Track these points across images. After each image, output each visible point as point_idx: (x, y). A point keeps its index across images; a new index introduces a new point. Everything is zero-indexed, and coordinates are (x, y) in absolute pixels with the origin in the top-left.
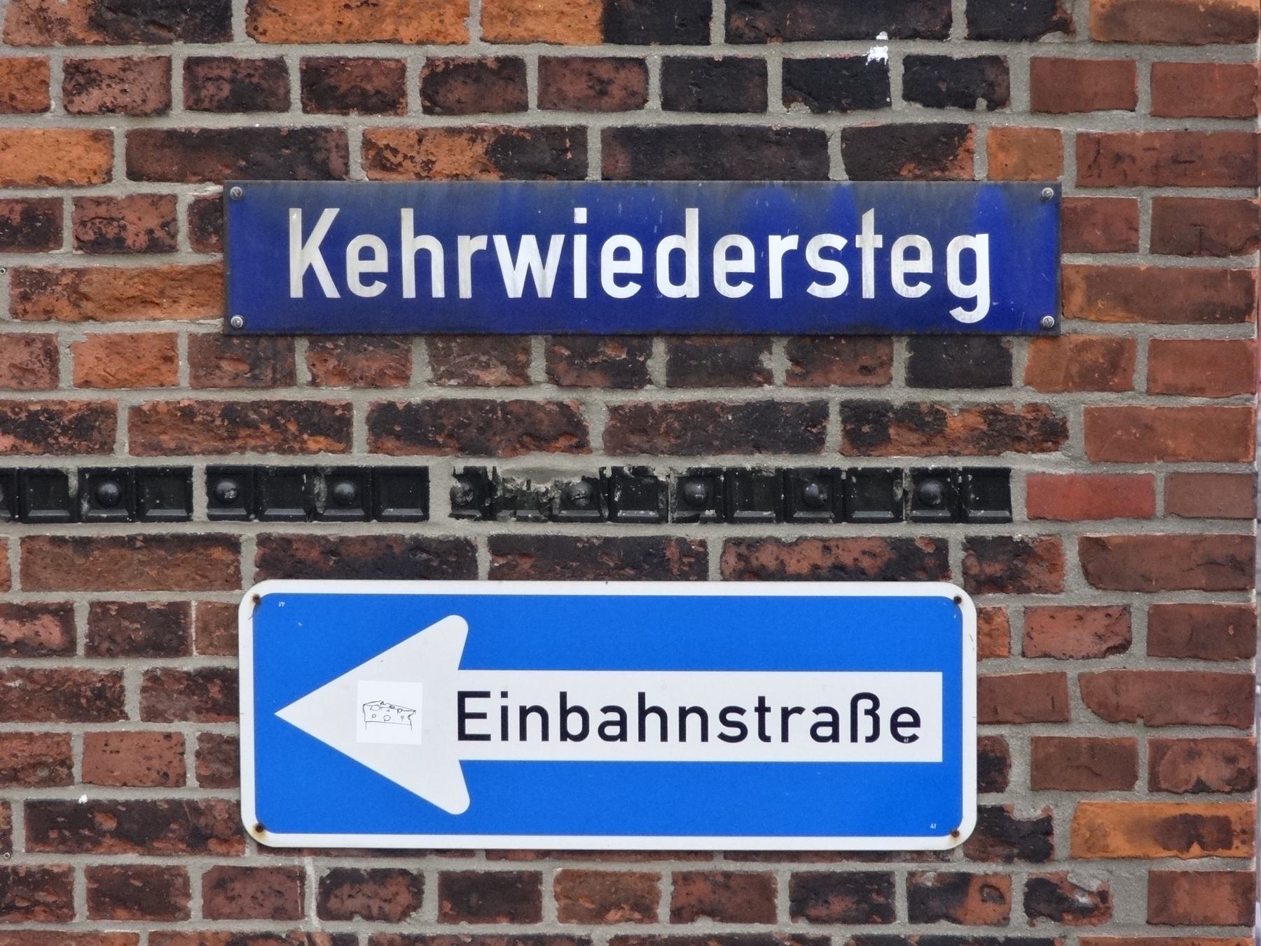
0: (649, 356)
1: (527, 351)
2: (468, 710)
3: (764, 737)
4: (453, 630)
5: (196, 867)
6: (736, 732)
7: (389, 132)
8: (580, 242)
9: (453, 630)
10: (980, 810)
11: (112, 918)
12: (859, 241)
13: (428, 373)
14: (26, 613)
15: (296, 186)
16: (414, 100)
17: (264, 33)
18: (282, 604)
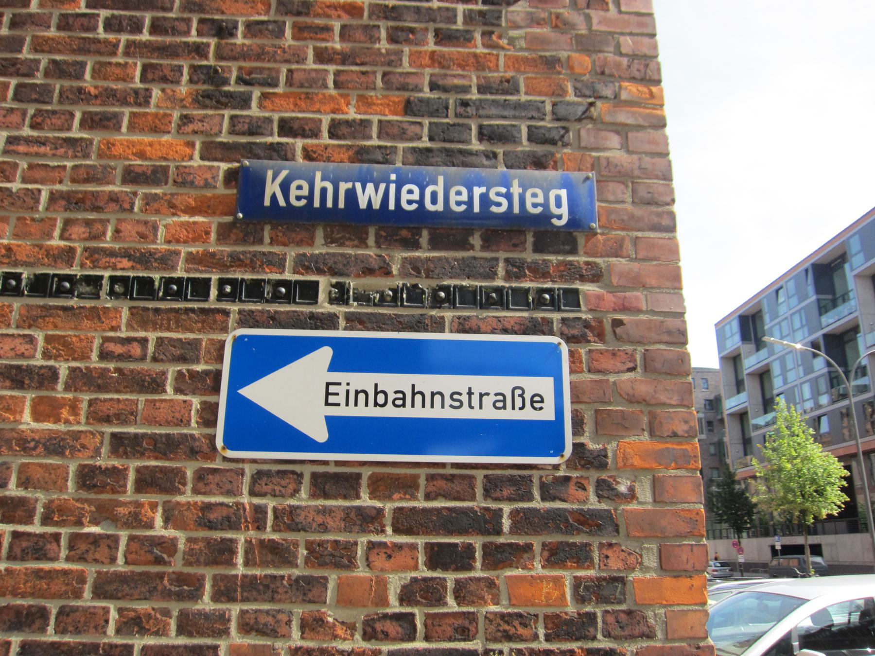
0: (421, 236)
1: (367, 233)
2: (330, 391)
3: (471, 407)
4: (325, 354)
5: (190, 470)
6: (457, 404)
7: (313, 145)
8: (393, 187)
9: (325, 354)
10: (574, 445)
11: (146, 493)
12: (512, 190)
13: (323, 242)
14: (129, 340)
15: (271, 162)
16: (325, 134)
17: (264, 107)
18: (551, 452)
